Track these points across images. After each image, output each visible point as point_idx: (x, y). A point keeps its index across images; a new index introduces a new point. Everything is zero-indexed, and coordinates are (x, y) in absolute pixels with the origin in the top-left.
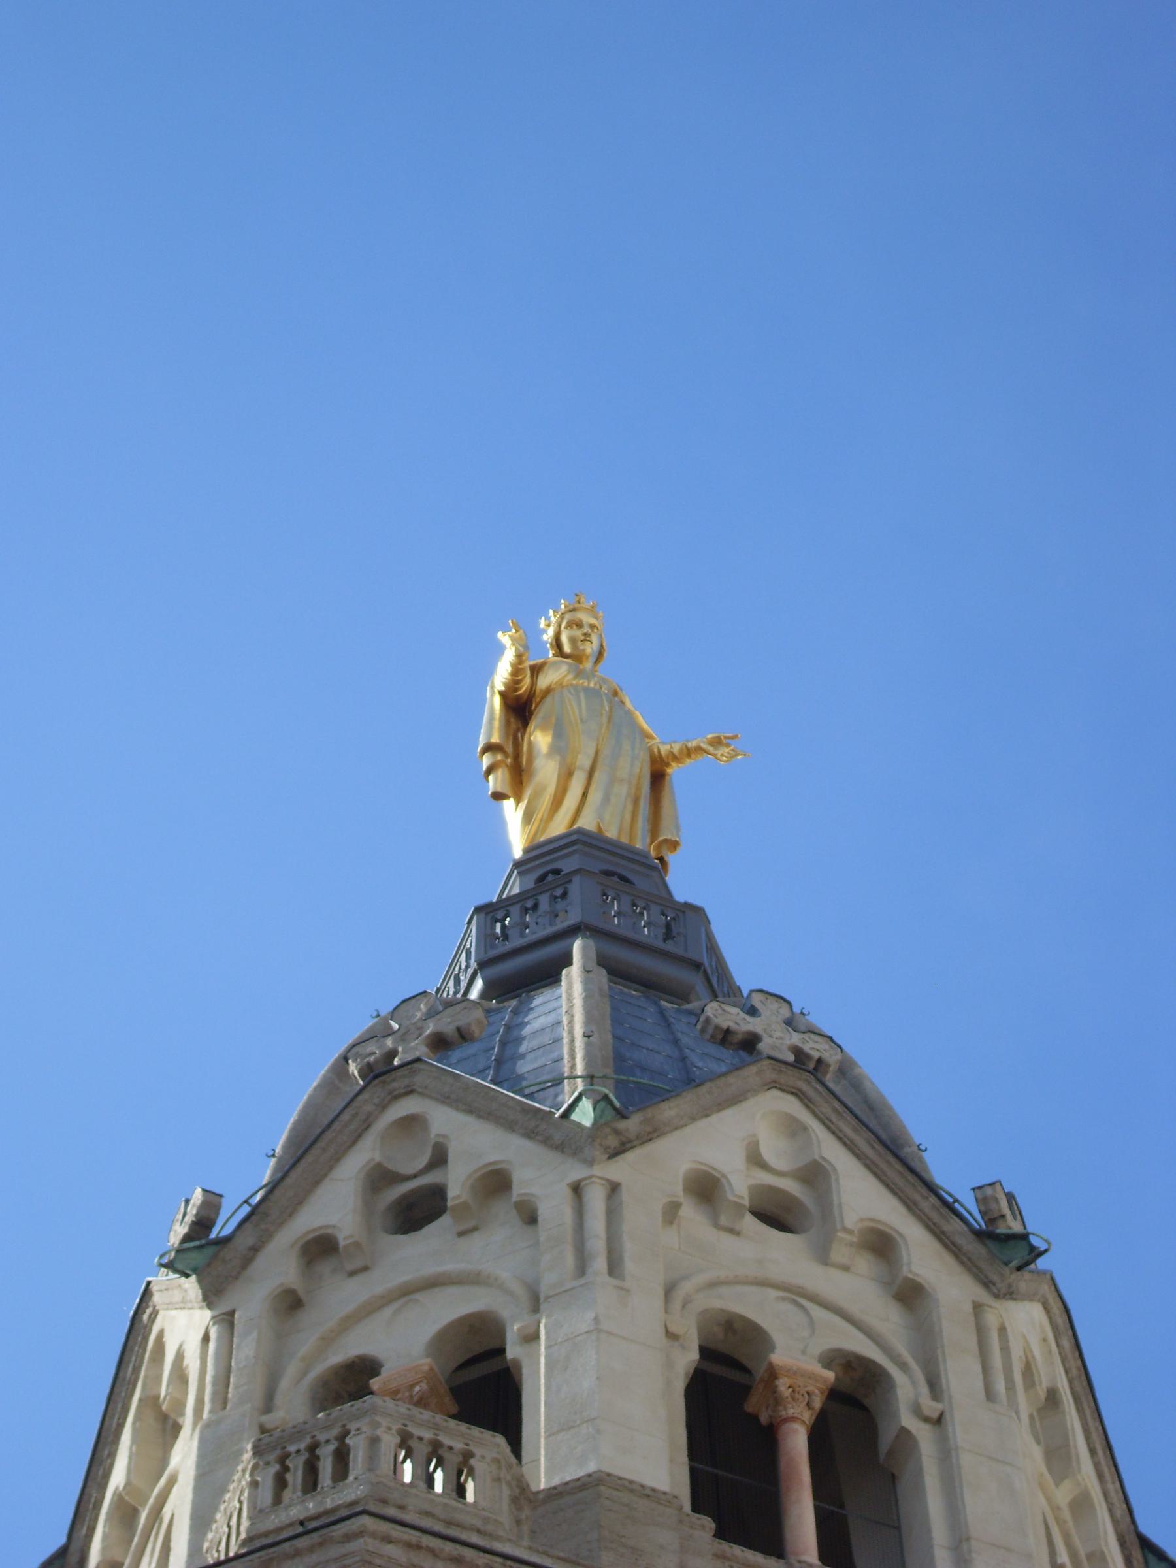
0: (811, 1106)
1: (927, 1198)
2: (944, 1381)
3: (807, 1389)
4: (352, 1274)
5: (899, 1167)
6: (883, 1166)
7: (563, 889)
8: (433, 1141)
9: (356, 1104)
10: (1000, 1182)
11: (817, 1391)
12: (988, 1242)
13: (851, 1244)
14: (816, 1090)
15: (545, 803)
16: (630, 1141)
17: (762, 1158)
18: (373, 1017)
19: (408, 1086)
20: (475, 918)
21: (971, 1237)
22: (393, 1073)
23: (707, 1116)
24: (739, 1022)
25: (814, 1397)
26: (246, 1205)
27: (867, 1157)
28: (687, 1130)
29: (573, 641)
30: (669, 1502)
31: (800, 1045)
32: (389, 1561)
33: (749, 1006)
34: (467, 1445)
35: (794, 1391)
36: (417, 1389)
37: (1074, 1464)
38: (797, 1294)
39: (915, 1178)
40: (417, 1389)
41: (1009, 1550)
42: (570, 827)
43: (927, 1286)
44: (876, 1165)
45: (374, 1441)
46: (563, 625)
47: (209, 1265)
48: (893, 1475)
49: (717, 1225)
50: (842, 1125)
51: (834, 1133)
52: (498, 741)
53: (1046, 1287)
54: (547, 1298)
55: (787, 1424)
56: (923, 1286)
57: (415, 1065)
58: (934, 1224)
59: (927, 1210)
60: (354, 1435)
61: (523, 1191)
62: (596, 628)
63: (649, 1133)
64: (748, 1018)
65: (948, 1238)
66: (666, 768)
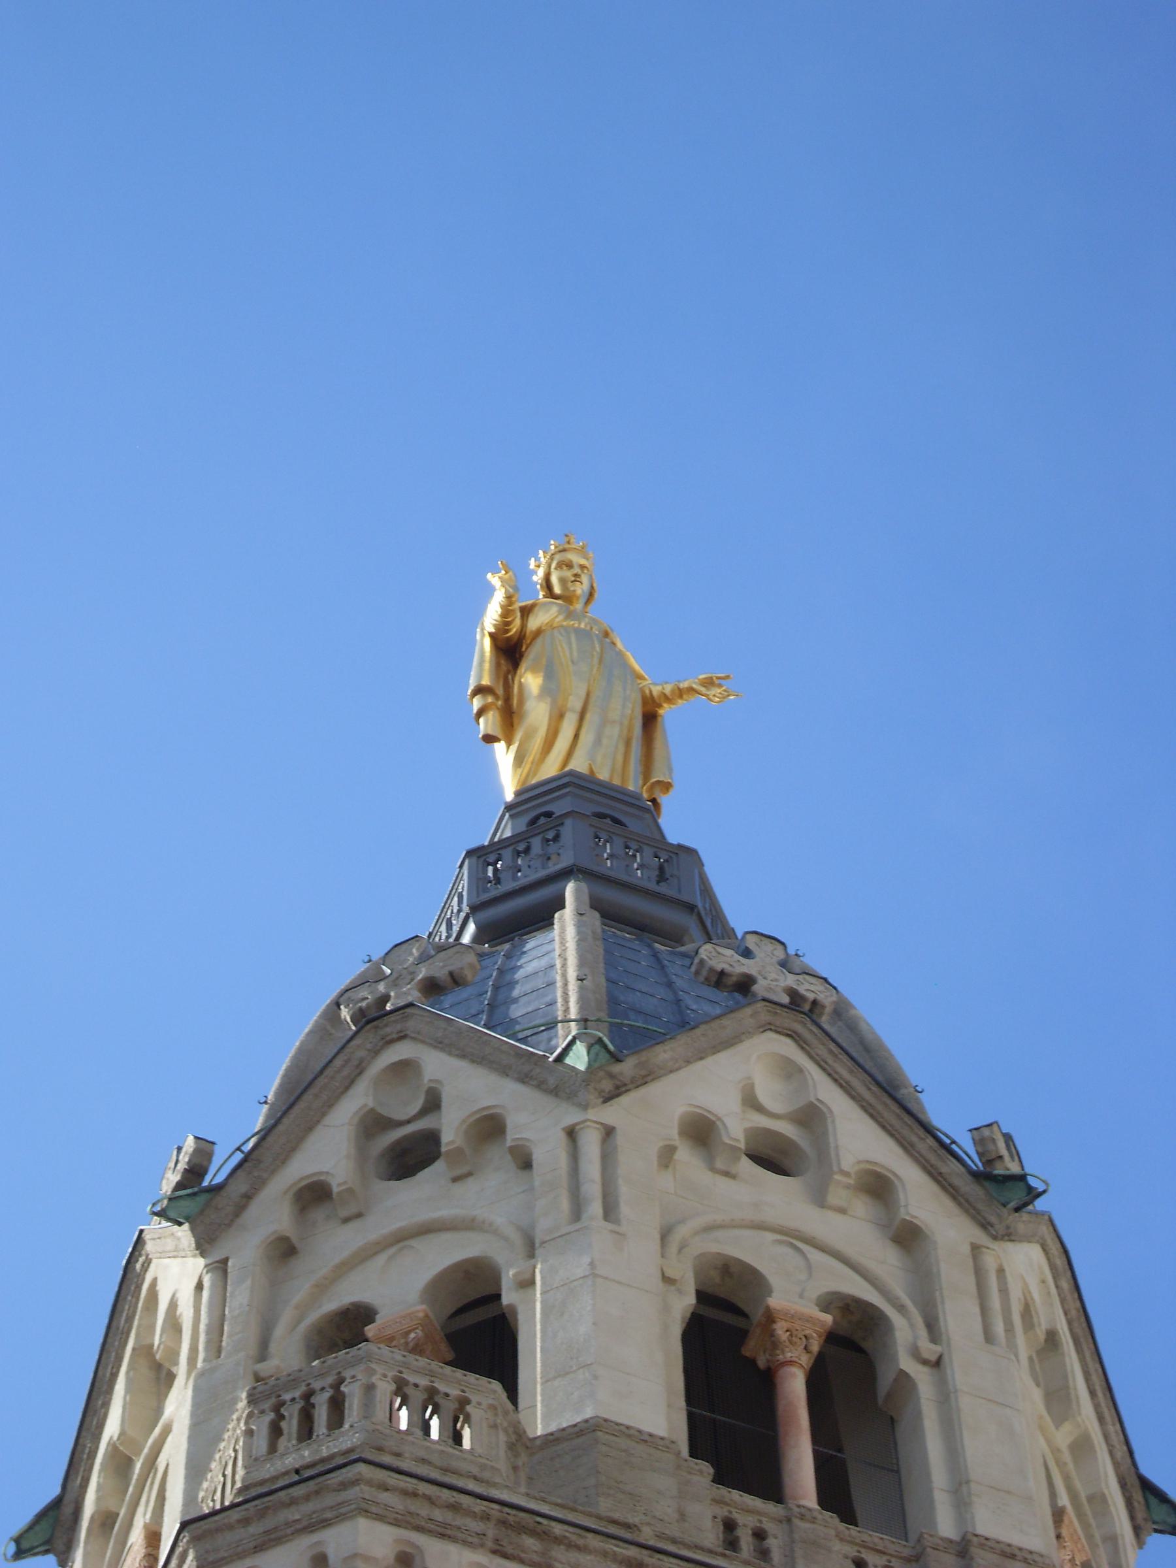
4: (346, 1220)
6: (880, 1107)
9: (347, 1050)
15: (536, 748)
16: (625, 1085)
18: (365, 963)
21: (969, 1178)
23: (701, 1058)
26: (238, 1152)
28: (682, 1073)
29: (563, 581)
33: (744, 948)
35: (791, 1335)
36: (412, 1335)
38: (794, 1237)
40: (412, 1335)
41: (1009, 1492)
43: (923, 1227)
45: (370, 1388)
47: (202, 1212)
49: (713, 1169)
51: (829, 1075)
52: (489, 683)
65: (945, 1180)
66: (657, 709)
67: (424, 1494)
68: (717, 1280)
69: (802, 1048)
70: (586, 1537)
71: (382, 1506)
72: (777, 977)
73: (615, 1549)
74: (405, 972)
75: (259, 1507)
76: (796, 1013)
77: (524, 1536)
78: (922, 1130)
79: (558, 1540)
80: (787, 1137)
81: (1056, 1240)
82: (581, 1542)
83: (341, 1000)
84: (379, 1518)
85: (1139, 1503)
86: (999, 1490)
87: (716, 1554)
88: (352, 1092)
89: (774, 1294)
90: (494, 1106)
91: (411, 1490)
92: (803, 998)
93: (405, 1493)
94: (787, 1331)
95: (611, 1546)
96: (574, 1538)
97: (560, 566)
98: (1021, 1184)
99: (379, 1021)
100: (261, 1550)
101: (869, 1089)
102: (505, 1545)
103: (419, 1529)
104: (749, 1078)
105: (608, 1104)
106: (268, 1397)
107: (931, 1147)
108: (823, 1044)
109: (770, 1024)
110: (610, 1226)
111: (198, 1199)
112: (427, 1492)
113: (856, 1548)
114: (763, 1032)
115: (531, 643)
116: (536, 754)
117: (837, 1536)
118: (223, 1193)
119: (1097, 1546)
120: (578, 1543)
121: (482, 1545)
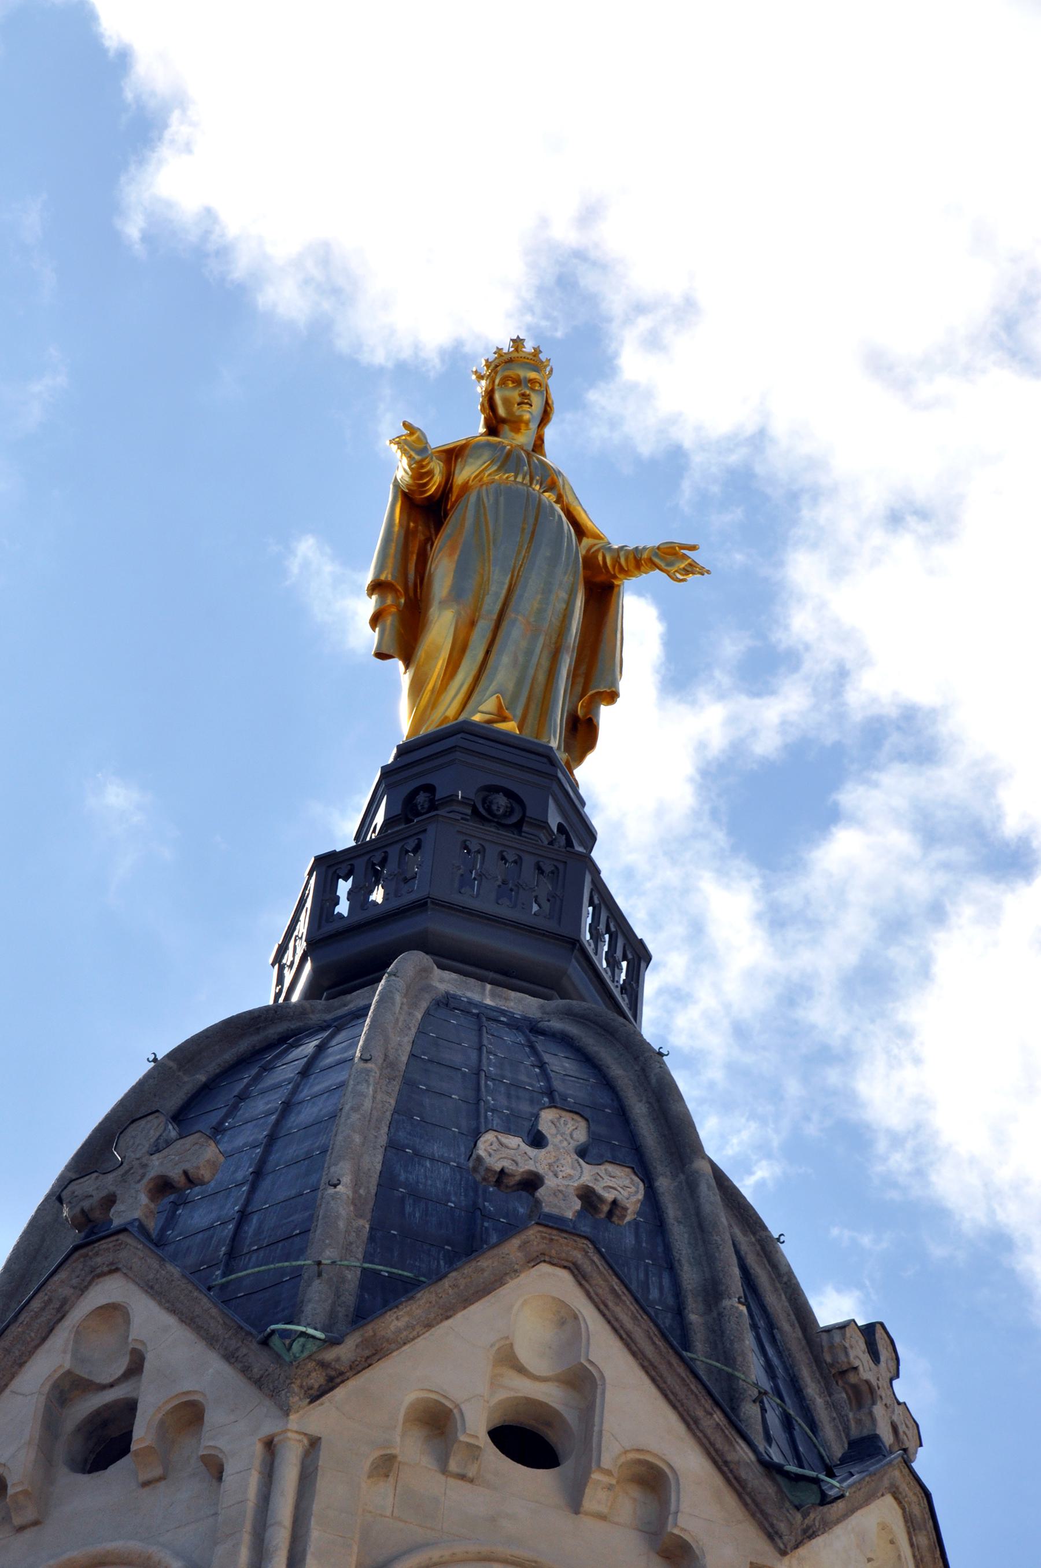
5: (681, 1370)
6: (663, 1368)
7: (416, 841)
9: (49, 1287)
13: (610, 1487)
15: (437, 670)
16: (342, 1374)
17: (520, 1362)
18: (150, 1062)
19: (112, 1264)
20: (383, 782)
21: (758, 1469)
23: (448, 1318)
24: (519, 1159)
28: (420, 1342)
29: (506, 402)
33: (536, 1130)
39: (700, 1387)
42: (456, 719)
44: (655, 1368)
46: (497, 381)
49: (444, 1471)
50: (618, 1310)
52: (390, 578)
53: (897, 1473)
58: (716, 1451)
62: (538, 385)
63: (368, 1357)
64: (532, 1152)
65: (731, 1471)
66: (613, 581)
69: (581, 1285)
72: (572, 1172)
74: (136, 1163)
78: (710, 1402)
81: (913, 1483)
83: (65, 1195)
90: (195, 1392)
92: (601, 1199)
97: (503, 382)
98: (814, 1487)
99: (89, 1248)
101: (654, 1343)
105: (318, 1402)
107: (718, 1424)
109: (543, 1254)
114: (534, 1266)
116: (436, 682)
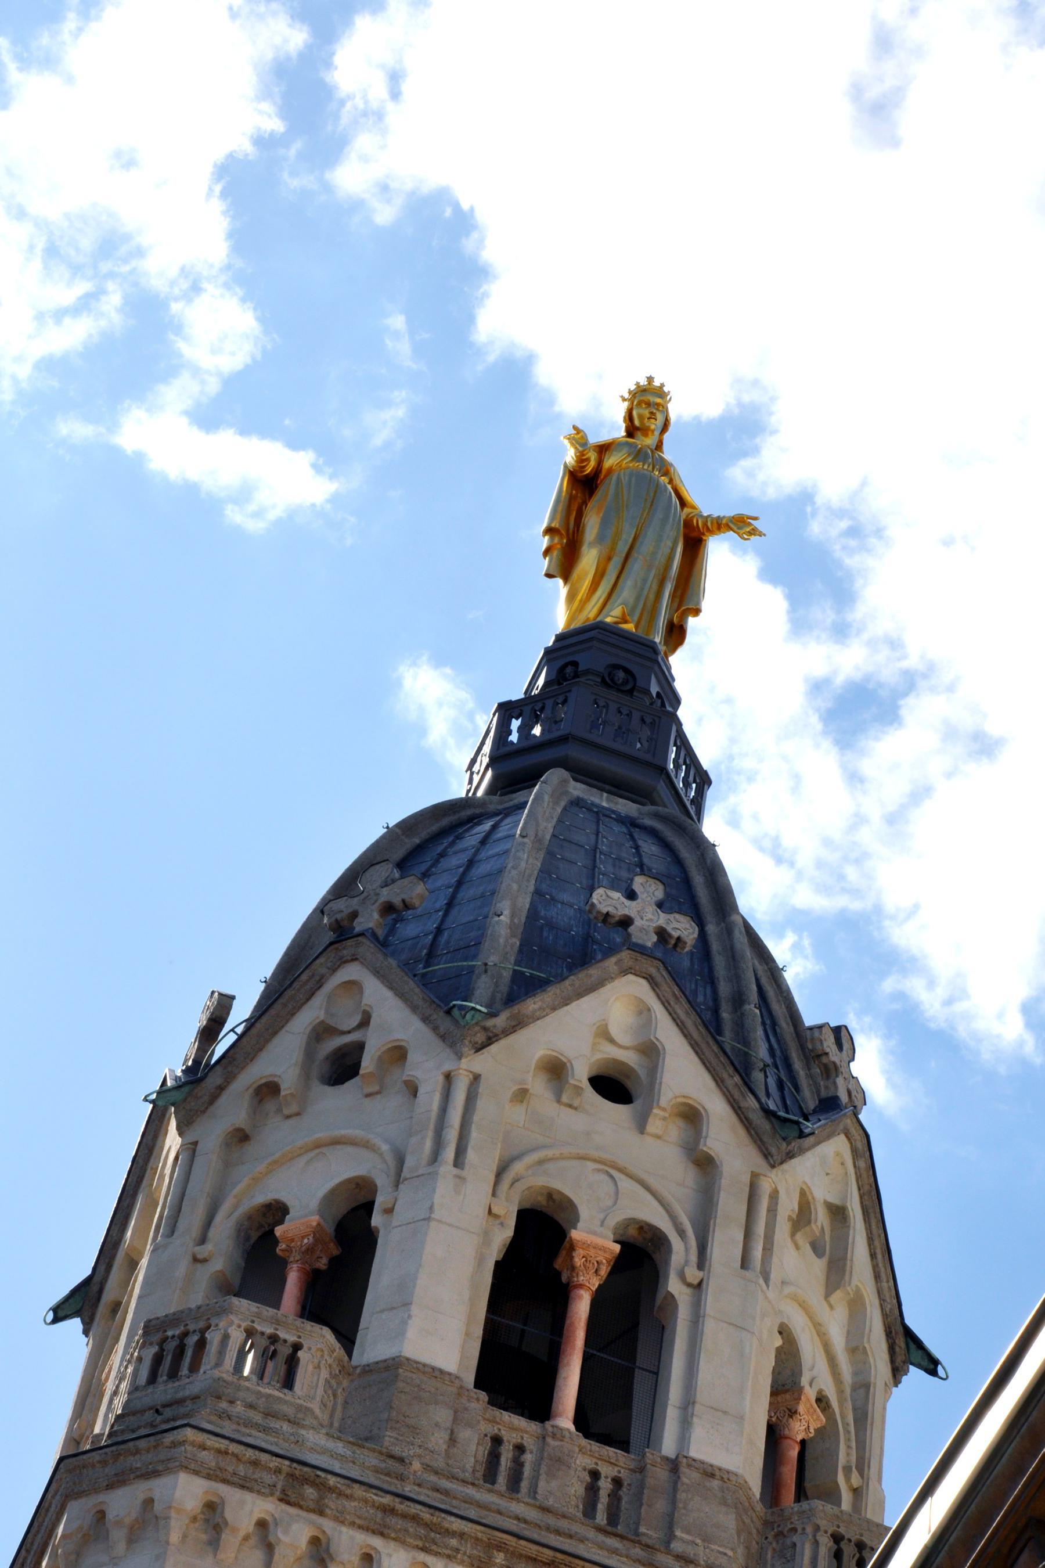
0: (656, 988)
1: (732, 1077)
2: (709, 1250)
3: (598, 1259)
4: (288, 1117)
6: (704, 1046)
8: (363, 1008)
9: (313, 967)
10: (828, 1023)
11: (604, 1261)
12: (773, 1119)
13: (664, 1119)
14: (662, 975)
15: (584, 587)
16: (496, 1035)
19: (354, 955)
21: (761, 1113)
22: (344, 942)
23: (567, 1004)
25: (601, 1266)
26: (232, 1033)
27: (692, 1037)
29: (640, 417)
30: (452, 1382)
31: (664, 926)
32: (202, 1466)
34: (299, 1337)
35: (586, 1261)
36: (306, 1241)
37: (847, 1277)
38: (612, 1168)
40: (306, 1241)
41: (725, 1413)
43: (716, 1158)
45: (226, 1337)
46: (635, 403)
47: (185, 1100)
48: (663, 1327)
50: (677, 1007)
51: (670, 1014)
52: (557, 526)
54: (406, 1179)
55: (576, 1290)
56: (713, 1158)
57: (360, 938)
58: (734, 1100)
59: (730, 1088)
60: (213, 1330)
61: (411, 1073)
65: (743, 1113)
67: (233, 1453)
68: (544, 1203)
69: (654, 990)
70: (352, 1487)
71: (199, 1463)
72: (652, 917)
73: (375, 1497)
75: (114, 1453)
76: (652, 959)
77: (306, 1487)
78: (732, 1069)
79: (331, 1490)
80: (629, 1066)
81: (859, 1128)
82: (348, 1492)
83: (326, 909)
84: (196, 1473)
85: (900, 1347)
86: (717, 1410)
87: (467, 1483)
88: (311, 1002)
89: (580, 1225)
90: (402, 1040)
91: (223, 1449)
93: (219, 1451)
94: (583, 1257)
95: (371, 1496)
96: (343, 1488)
98: (796, 1127)
99: (339, 944)
100: (112, 1488)
101: (698, 1030)
102: (289, 1494)
103: (225, 1481)
104: (604, 1020)
106: (158, 1330)
107: (736, 1084)
108: (670, 988)
110: (455, 1171)
111: (183, 1089)
112: (236, 1452)
113: (595, 1460)
114: (624, 976)
115: (603, 479)
117: (580, 1450)
118: (203, 1084)
119: (846, 1400)
120: (346, 1492)
121: (272, 1495)
